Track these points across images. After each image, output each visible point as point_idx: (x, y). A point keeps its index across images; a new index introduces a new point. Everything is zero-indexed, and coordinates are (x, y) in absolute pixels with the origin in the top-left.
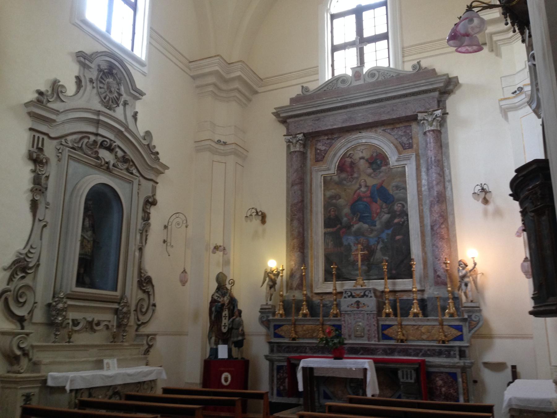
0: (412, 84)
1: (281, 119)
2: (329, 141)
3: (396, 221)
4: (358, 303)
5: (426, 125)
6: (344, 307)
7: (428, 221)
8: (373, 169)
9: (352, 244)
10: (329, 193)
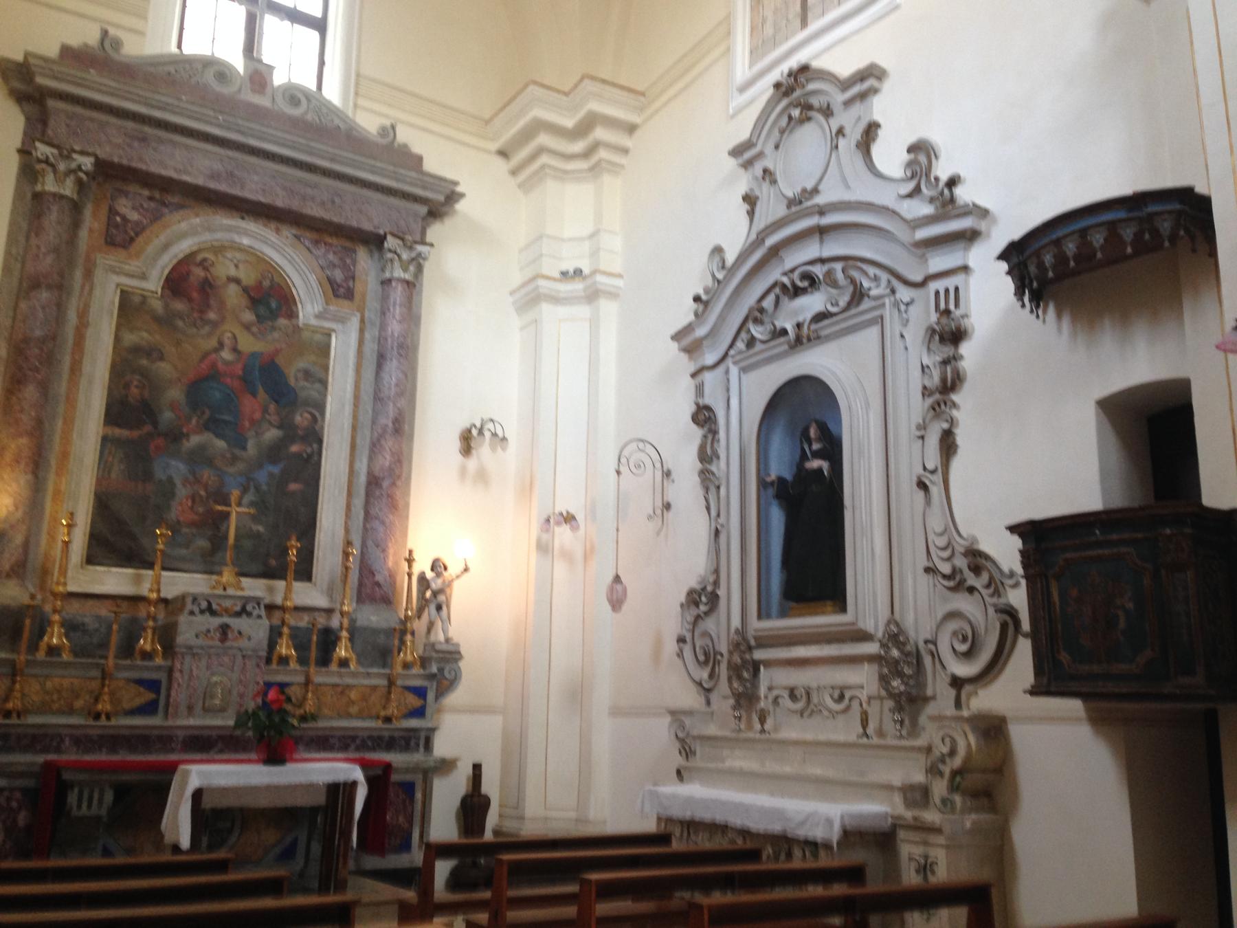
2: (152, 205)
3: (294, 448)
4: (224, 629)
5: (397, 264)
8: (257, 316)
9: (178, 482)
10: (130, 338)
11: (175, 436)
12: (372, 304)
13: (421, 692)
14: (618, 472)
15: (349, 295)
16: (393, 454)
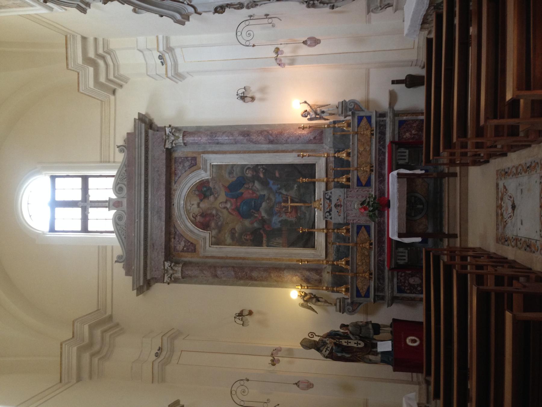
0: (137, 150)
1: (145, 287)
2: (177, 237)
3: (262, 175)
4: (336, 206)
5: (177, 142)
6: (340, 220)
7: (265, 147)
9: (280, 219)
10: (229, 240)
11: (263, 221)
13: (360, 119)
14: (254, 46)
15: (194, 159)
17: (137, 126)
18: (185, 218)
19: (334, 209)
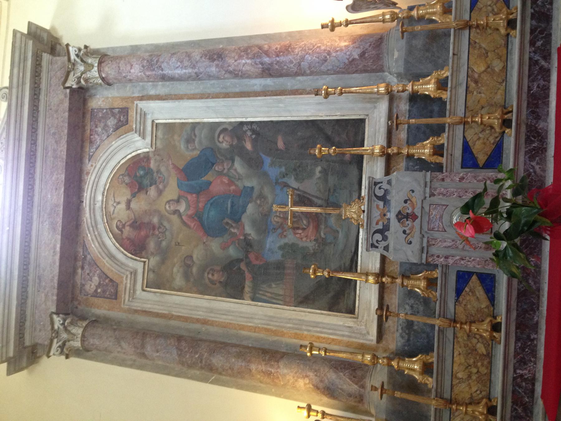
2: (86, 267)
3: (249, 146)
4: (401, 216)
5: (88, 75)
6: (411, 254)
9: (283, 241)
10: (179, 281)
11: (247, 245)
12: (129, 91)
16: (240, 57)
17: (18, 44)
18: (103, 229)
19: (394, 225)
